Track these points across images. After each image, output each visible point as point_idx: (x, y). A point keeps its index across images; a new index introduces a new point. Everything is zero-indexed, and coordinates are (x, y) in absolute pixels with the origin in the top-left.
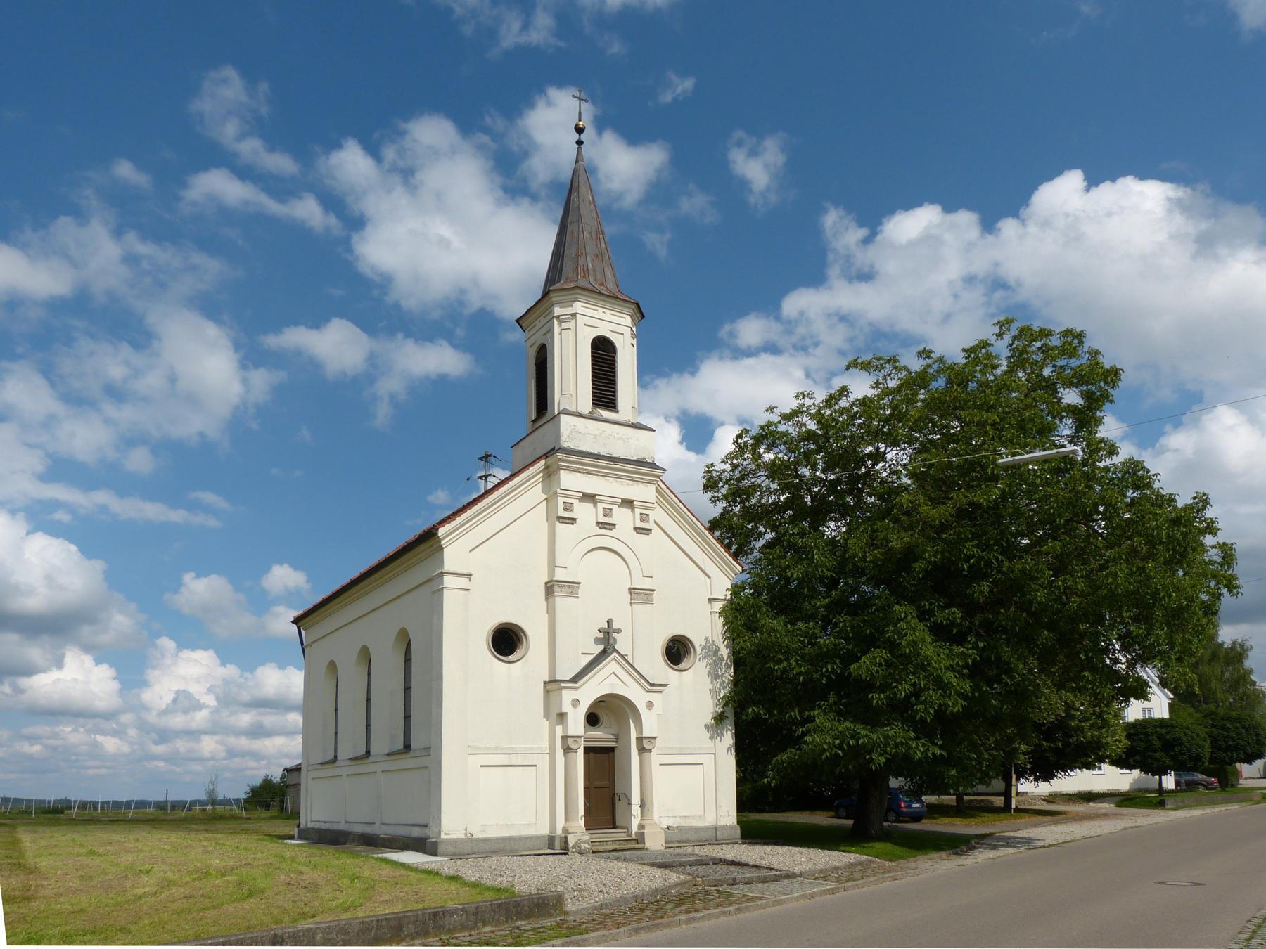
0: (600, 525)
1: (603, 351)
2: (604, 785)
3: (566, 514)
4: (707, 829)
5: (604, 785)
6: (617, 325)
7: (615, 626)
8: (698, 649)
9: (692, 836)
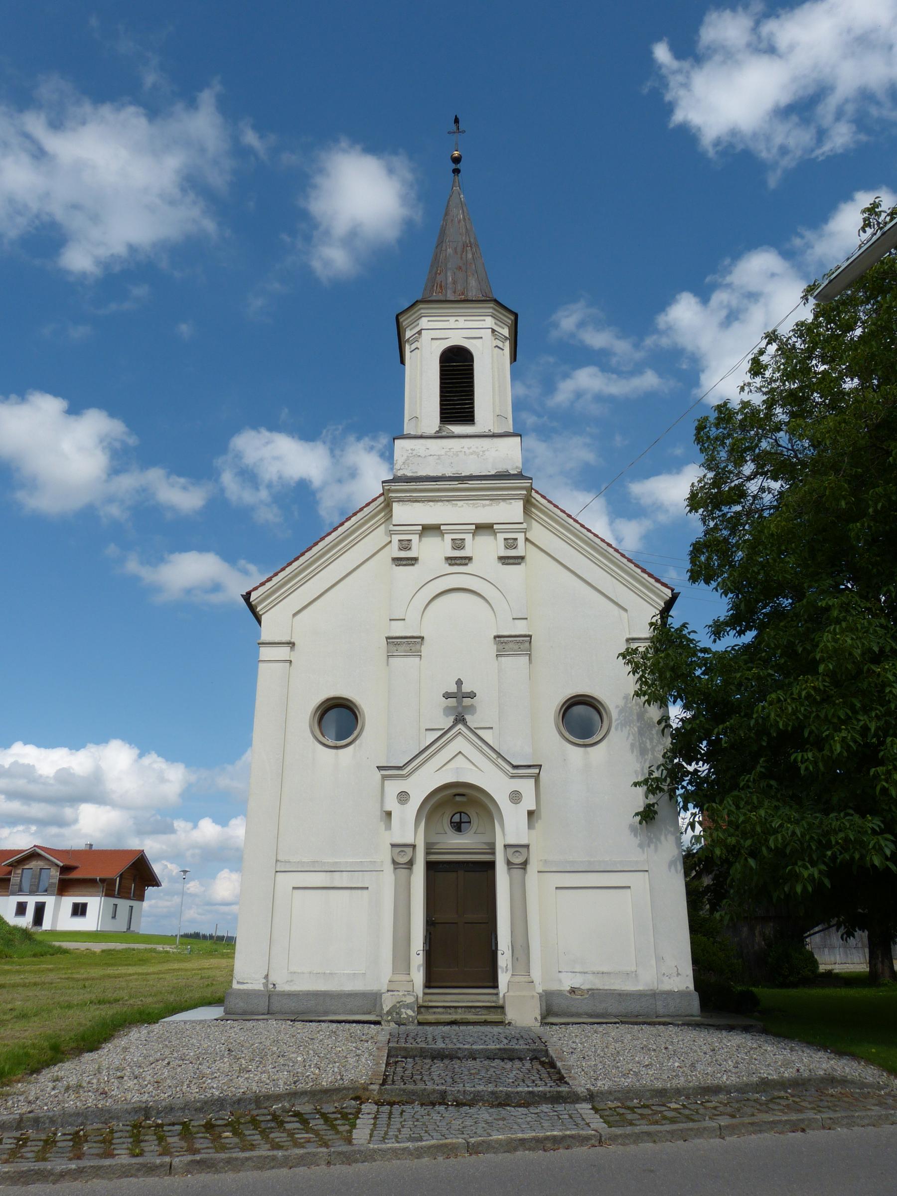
0: (398, 561)
1: (457, 368)
2: (460, 912)
3: (403, 554)
4: (640, 995)
5: (460, 912)
6: (479, 333)
7: (466, 688)
8: (614, 714)
9: (613, 1007)
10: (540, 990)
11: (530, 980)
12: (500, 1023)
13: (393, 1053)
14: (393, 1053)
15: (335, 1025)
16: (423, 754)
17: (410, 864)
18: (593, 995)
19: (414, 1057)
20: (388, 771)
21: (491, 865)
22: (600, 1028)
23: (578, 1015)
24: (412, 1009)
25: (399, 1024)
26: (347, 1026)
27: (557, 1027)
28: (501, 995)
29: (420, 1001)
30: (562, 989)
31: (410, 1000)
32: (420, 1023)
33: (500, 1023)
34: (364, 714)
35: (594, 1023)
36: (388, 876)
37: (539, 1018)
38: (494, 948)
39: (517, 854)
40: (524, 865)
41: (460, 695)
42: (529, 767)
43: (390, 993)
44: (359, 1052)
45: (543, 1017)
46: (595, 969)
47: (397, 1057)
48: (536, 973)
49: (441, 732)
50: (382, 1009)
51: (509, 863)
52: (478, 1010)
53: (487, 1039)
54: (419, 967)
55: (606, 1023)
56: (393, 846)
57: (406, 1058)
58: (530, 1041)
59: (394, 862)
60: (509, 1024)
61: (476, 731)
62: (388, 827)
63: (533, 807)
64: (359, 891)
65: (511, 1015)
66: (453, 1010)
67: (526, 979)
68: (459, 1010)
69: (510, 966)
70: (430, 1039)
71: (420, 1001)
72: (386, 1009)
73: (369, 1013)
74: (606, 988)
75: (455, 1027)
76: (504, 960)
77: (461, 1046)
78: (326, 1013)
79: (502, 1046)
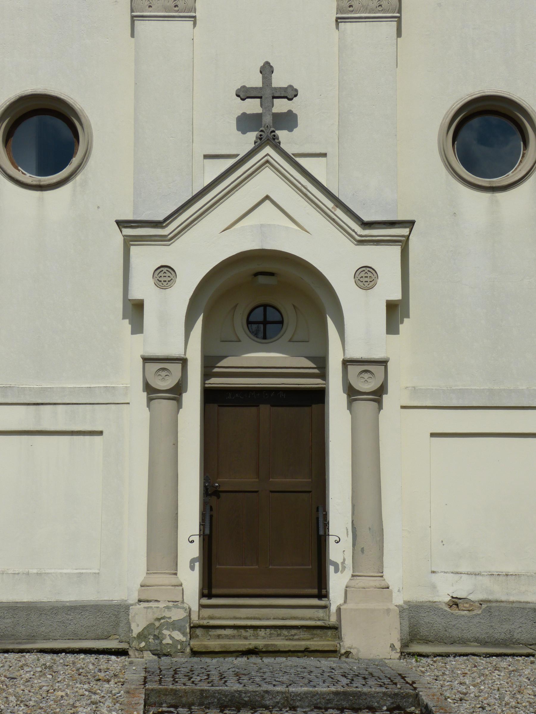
7: (279, 81)
10: (398, 599)
11: (383, 584)
12: (333, 653)
13: (152, 700)
14: (152, 700)
15: (48, 657)
16: (199, 201)
17: (177, 392)
18: (489, 610)
19: (189, 706)
20: (137, 230)
21: (319, 396)
22: (504, 663)
23: (464, 642)
24: (181, 630)
25: (159, 654)
26: (70, 658)
27: (429, 660)
28: (333, 608)
29: (195, 618)
30: (436, 599)
31: (177, 615)
32: (195, 653)
33: (333, 653)
34: (90, 126)
35: (491, 655)
36: (138, 412)
37: (398, 645)
38: (321, 533)
39: (366, 376)
40: (379, 394)
41: (268, 94)
42: (392, 224)
43: (143, 605)
44: (95, 698)
45: (405, 645)
46: (494, 569)
47: (160, 705)
48: (394, 573)
49: (231, 162)
50: (130, 630)
51: (351, 392)
52: (293, 632)
53: (312, 677)
54: (193, 561)
55: (513, 655)
56: (146, 360)
57: (176, 707)
58: (387, 681)
59: (148, 388)
60: (347, 654)
61: (298, 160)
62: (138, 327)
63: (396, 295)
64: (87, 438)
65: (350, 640)
66: (251, 631)
67: (376, 582)
68: (262, 633)
69: (349, 562)
70: (215, 677)
71: (195, 618)
72: (136, 630)
73: (107, 638)
74: (512, 599)
75: (254, 659)
76: (339, 550)
77: (270, 688)
78: (32, 638)
79: (340, 689)
